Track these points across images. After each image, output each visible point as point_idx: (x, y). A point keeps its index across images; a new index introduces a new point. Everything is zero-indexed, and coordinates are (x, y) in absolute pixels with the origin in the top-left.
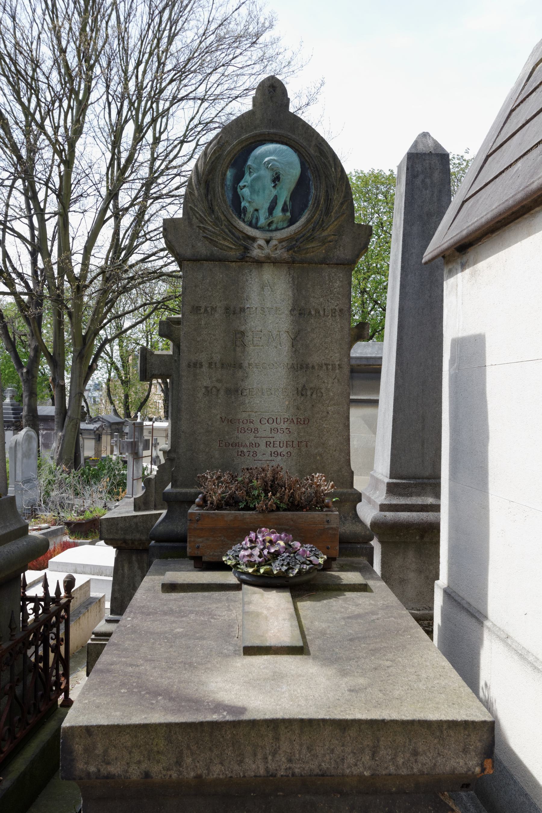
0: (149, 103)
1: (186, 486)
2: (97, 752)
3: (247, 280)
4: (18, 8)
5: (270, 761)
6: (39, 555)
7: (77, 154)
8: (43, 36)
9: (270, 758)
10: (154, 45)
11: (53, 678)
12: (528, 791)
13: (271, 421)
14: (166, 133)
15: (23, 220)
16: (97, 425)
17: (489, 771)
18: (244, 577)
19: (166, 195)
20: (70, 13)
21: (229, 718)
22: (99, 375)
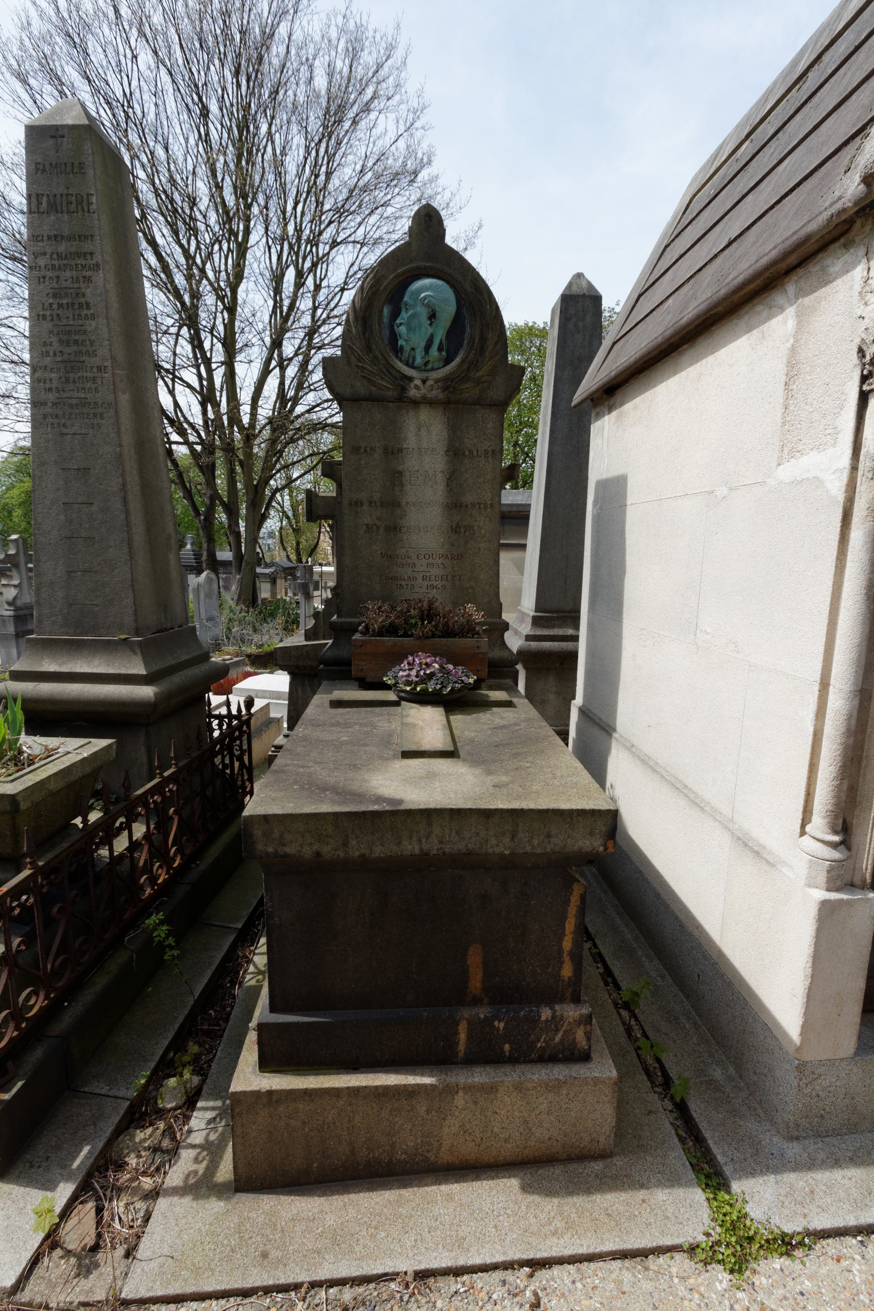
0: (309, 246)
1: (350, 616)
2: (274, 836)
3: (404, 421)
4: (171, 137)
5: (424, 843)
6: (222, 680)
7: (240, 301)
8: (198, 169)
9: (424, 840)
10: (312, 182)
11: (239, 783)
12: (642, 869)
13: (427, 557)
14: (326, 279)
15: (190, 369)
16: (272, 570)
17: (611, 850)
18: (402, 694)
19: (328, 344)
20: (224, 144)
21: (387, 808)
22: (272, 523)
